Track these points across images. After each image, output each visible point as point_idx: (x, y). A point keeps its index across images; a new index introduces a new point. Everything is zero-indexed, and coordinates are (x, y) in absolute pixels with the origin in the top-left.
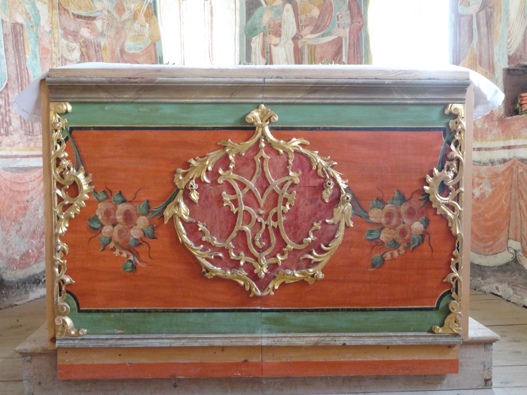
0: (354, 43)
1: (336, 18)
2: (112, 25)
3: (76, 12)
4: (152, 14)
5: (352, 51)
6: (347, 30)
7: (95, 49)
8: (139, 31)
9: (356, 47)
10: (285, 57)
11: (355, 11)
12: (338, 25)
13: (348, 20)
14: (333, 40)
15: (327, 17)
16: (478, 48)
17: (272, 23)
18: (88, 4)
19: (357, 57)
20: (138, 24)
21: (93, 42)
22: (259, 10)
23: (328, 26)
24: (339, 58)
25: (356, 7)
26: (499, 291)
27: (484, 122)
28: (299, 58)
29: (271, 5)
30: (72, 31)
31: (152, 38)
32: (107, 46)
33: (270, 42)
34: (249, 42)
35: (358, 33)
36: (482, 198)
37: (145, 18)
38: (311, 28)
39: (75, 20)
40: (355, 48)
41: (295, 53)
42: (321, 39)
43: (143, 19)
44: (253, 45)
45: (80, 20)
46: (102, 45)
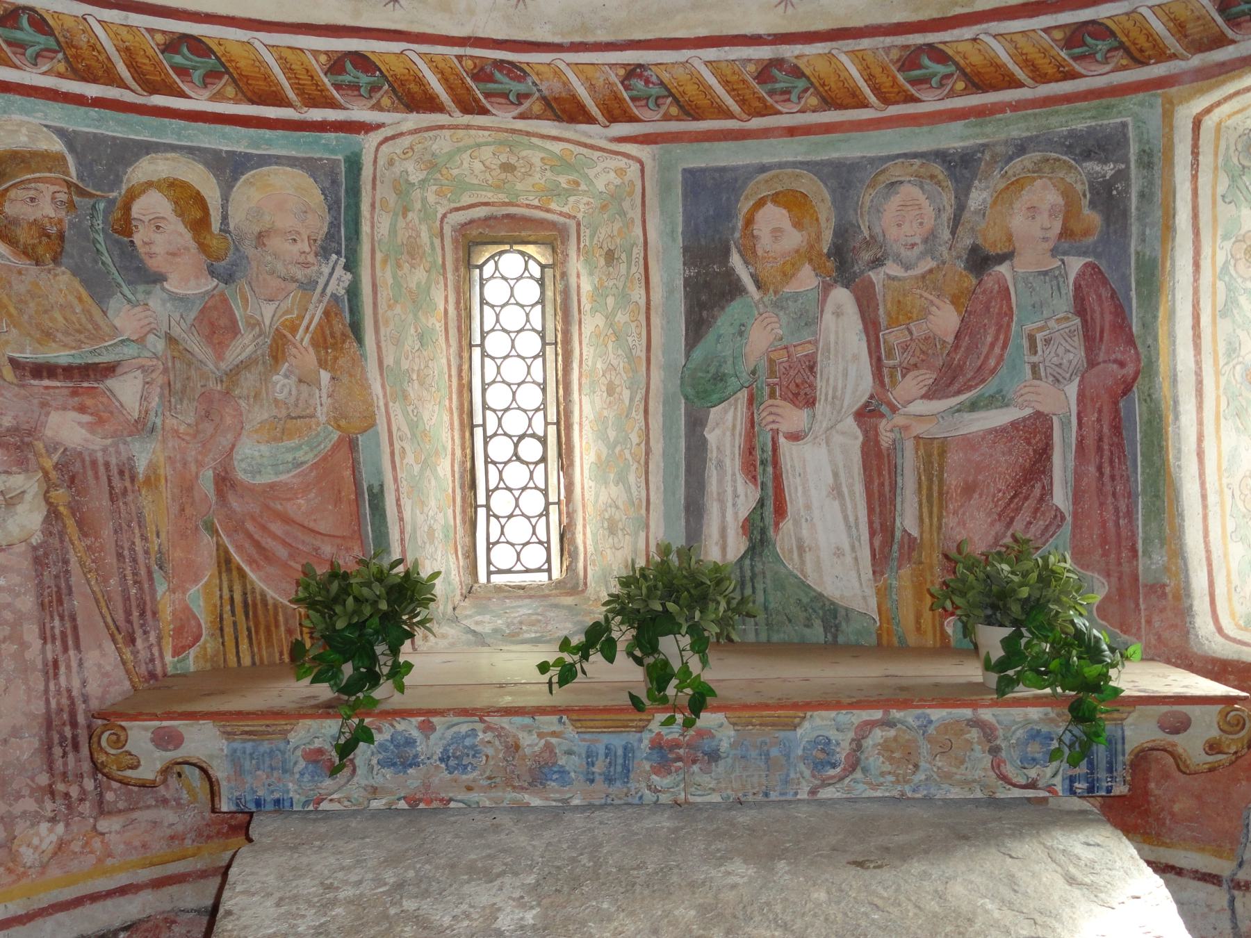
0: (1100, 439)
1: (1025, 343)
2: (184, 387)
3: (28, 354)
4: (343, 334)
5: (1092, 469)
6: (1072, 390)
7: (111, 488)
8: (293, 399)
9: (1107, 453)
10: (831, 480)
11: (1103, 316)
12: (1034, 368)
13: (1075, 354)
14: (1014, 424)
15: (989, 339)
17: (781, 357)
18: (84, 320)
20: (286, 376)
21: (101, 461)
22: (735, 309)
23: (993, 371)
24: (1037, 491)
25: (1107, 305)
29: (776, 292)
30: (8, 430)
31: (343, 423)
32: (162, 472)
33: (774, 426)
34: (696, 424)
35: (1116, 403)
37: (318, 353)
38: (926, 377)
39: (23, 386)
41: (866, 467)
42: (967, 416)
43: (311, 357)
44: (712, 436)
45: (46, 382)
46: (141, 466)
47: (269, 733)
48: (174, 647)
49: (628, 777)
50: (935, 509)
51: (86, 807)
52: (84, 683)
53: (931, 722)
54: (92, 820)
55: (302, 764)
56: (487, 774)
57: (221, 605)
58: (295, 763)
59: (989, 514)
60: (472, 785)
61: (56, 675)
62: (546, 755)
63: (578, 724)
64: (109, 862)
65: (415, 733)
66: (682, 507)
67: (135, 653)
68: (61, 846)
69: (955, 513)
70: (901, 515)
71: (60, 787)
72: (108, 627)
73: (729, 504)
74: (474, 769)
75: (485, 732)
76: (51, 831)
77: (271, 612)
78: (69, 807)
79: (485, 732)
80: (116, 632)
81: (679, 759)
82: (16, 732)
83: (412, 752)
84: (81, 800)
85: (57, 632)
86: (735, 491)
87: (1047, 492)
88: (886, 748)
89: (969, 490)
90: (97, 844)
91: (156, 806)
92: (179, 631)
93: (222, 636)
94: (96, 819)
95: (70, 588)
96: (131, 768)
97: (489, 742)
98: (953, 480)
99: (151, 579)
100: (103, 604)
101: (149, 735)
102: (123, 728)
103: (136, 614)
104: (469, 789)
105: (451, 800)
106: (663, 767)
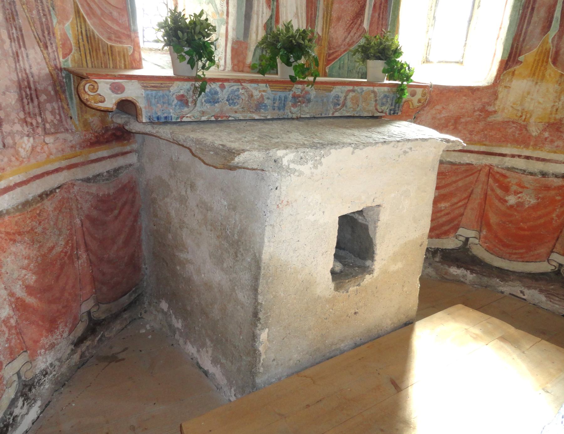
5: (377, 15)
16: (555, 42)
19: (382, 24)
24: (359, 21)
26: (524, 295)
27: (544, 130)
28: (312, 14)
36: (518, 206)
40: (381, 12)
47: (162, 87)
48: (63, 54)
49: (284, 108)
50: (328, 25)
51: (40, 130)
52: (30, 66)
53: (363, 91)
54: (43, 137)
55: (176, 101)
56: (242, 106)
57: (78, 35)
58: (173, 101)
59: (344, 29)
60: (237, 110)
61: (18, 60)
62: (261, 99)
63: (272, 88)
64: (52, 157)
65: (218, 89)
66: (244, 16)
67: (48, 54)
68: (33, 148)
69: (334, 27)
70: (317, 27)
71: (29, 120)
72: (35, 37)
73: (260, 16)
74: (238, 104)
75: (242, 89)
76: (28, 141)
77: (97, 42)
78: (33, 130)
79: (242, 89)
80: (39, 42)
81: (299, 102)
82: (7, 89)
83: (216, 97)
84: (37, 127)
85: (15, 36)
86: (263, 11)
87: (362, 22)
88: (352, 99)
89: (339, 19)
90: (46, 148)
91: (65, 132)
92: (64, 45)
93: (80, 51)
94: (44, 136)
95: (16, 12)
96: (101, 102)
97: (243, 94)
98: (334, 15)
99: (50, 15)
100: (32, 24)
101: (109, 86)
102: (96, 82)
103: (46, 33)
104: (236, 112)
105: (230, 117)
106: (294, 105)
